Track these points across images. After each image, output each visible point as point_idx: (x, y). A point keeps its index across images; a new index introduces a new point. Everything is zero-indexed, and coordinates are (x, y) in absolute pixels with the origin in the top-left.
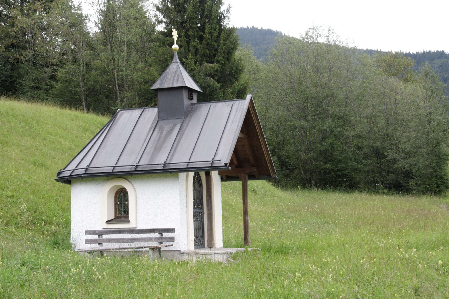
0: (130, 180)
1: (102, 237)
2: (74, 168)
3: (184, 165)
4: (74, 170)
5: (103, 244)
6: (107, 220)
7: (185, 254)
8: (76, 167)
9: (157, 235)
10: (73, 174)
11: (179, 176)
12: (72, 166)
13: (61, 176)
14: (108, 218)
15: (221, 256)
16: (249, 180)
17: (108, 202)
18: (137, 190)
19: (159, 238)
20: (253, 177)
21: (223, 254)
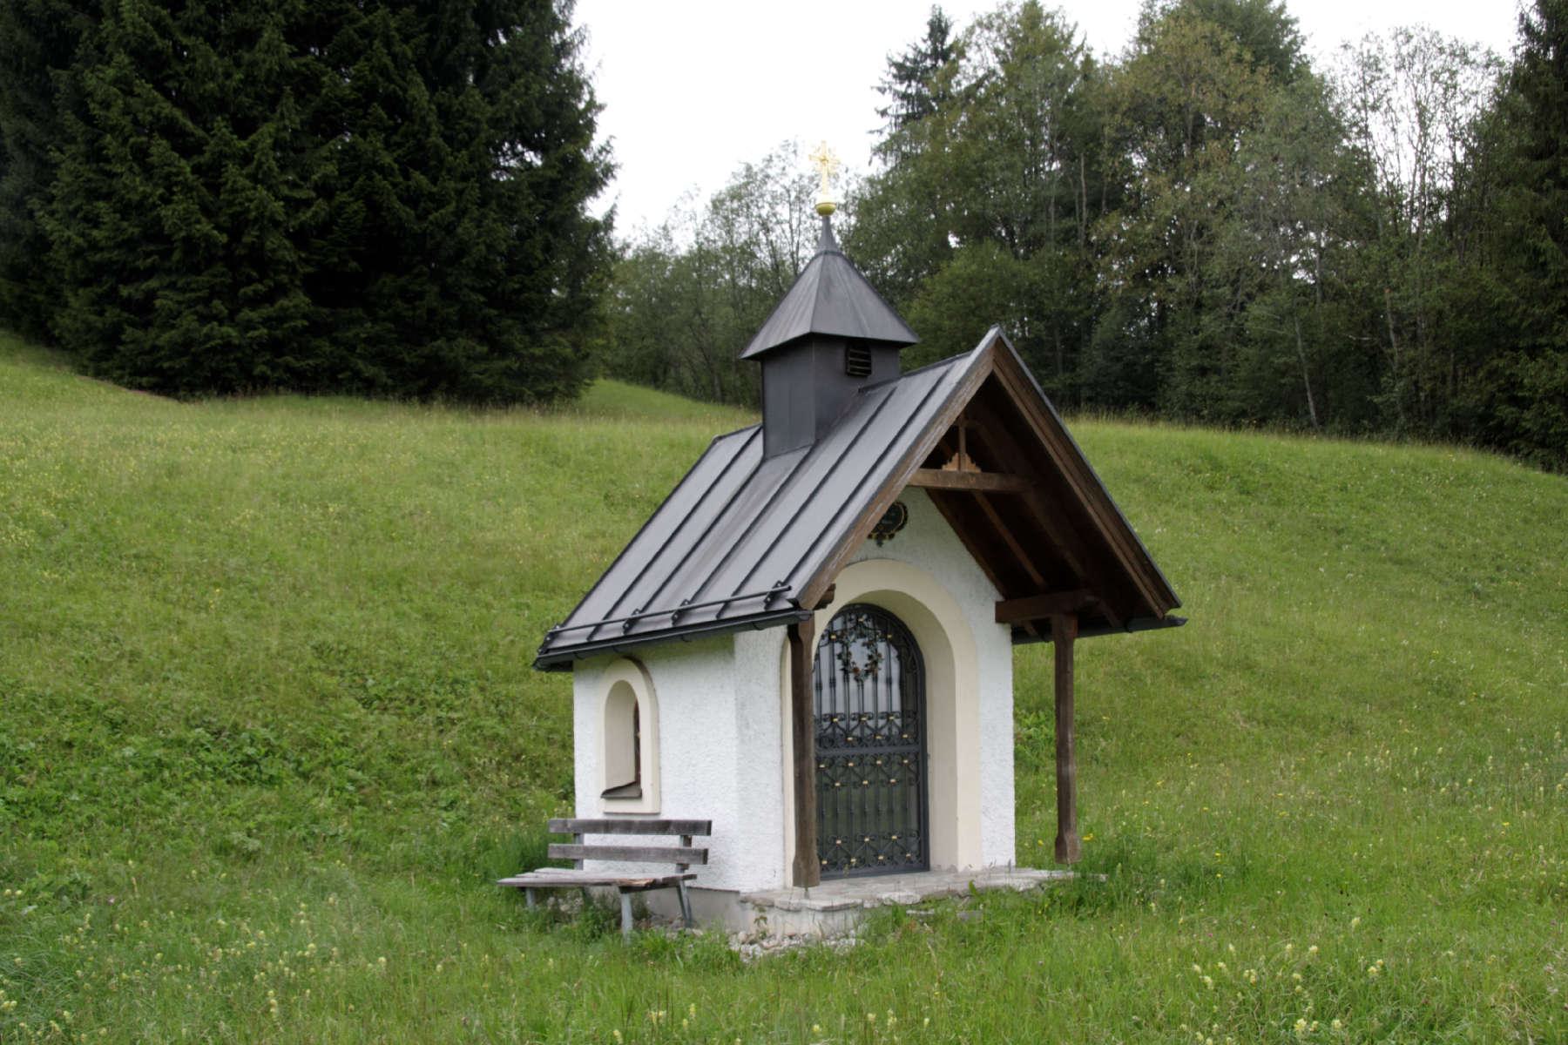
0: (649, 666)
1: (581, 842)
2: (599, 620)
3: (614, 630)
4: (727, 604)
5: (586, 862)
6: (604, 788)
7: (749, 905)
8: (736, 593)
9: (673, 841)
10: (597, 638)
11: (737, 648)
12: (593, 612)
13: (637, 630)
14: (608, 779)
15: (820, 917)
16: (1079, 636)
17: (609, 730)
18: (659, 693)
19: (680, 852)
20: (1093, 624)
21: (844, 908)
